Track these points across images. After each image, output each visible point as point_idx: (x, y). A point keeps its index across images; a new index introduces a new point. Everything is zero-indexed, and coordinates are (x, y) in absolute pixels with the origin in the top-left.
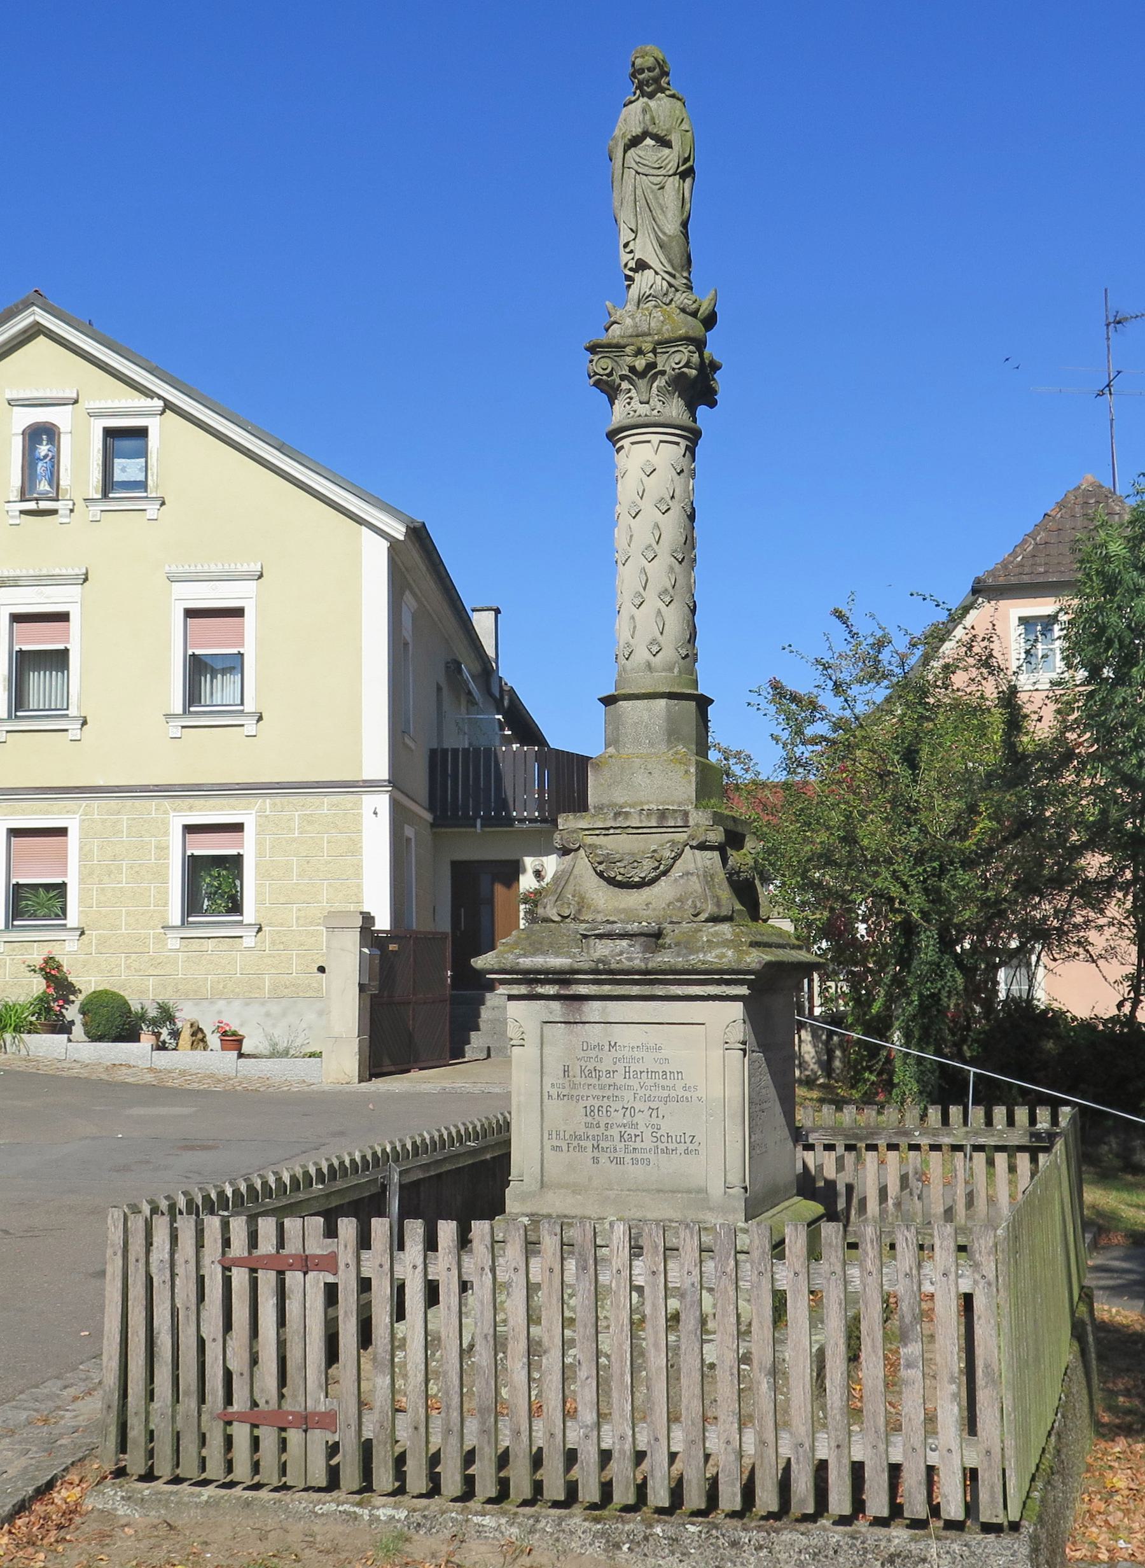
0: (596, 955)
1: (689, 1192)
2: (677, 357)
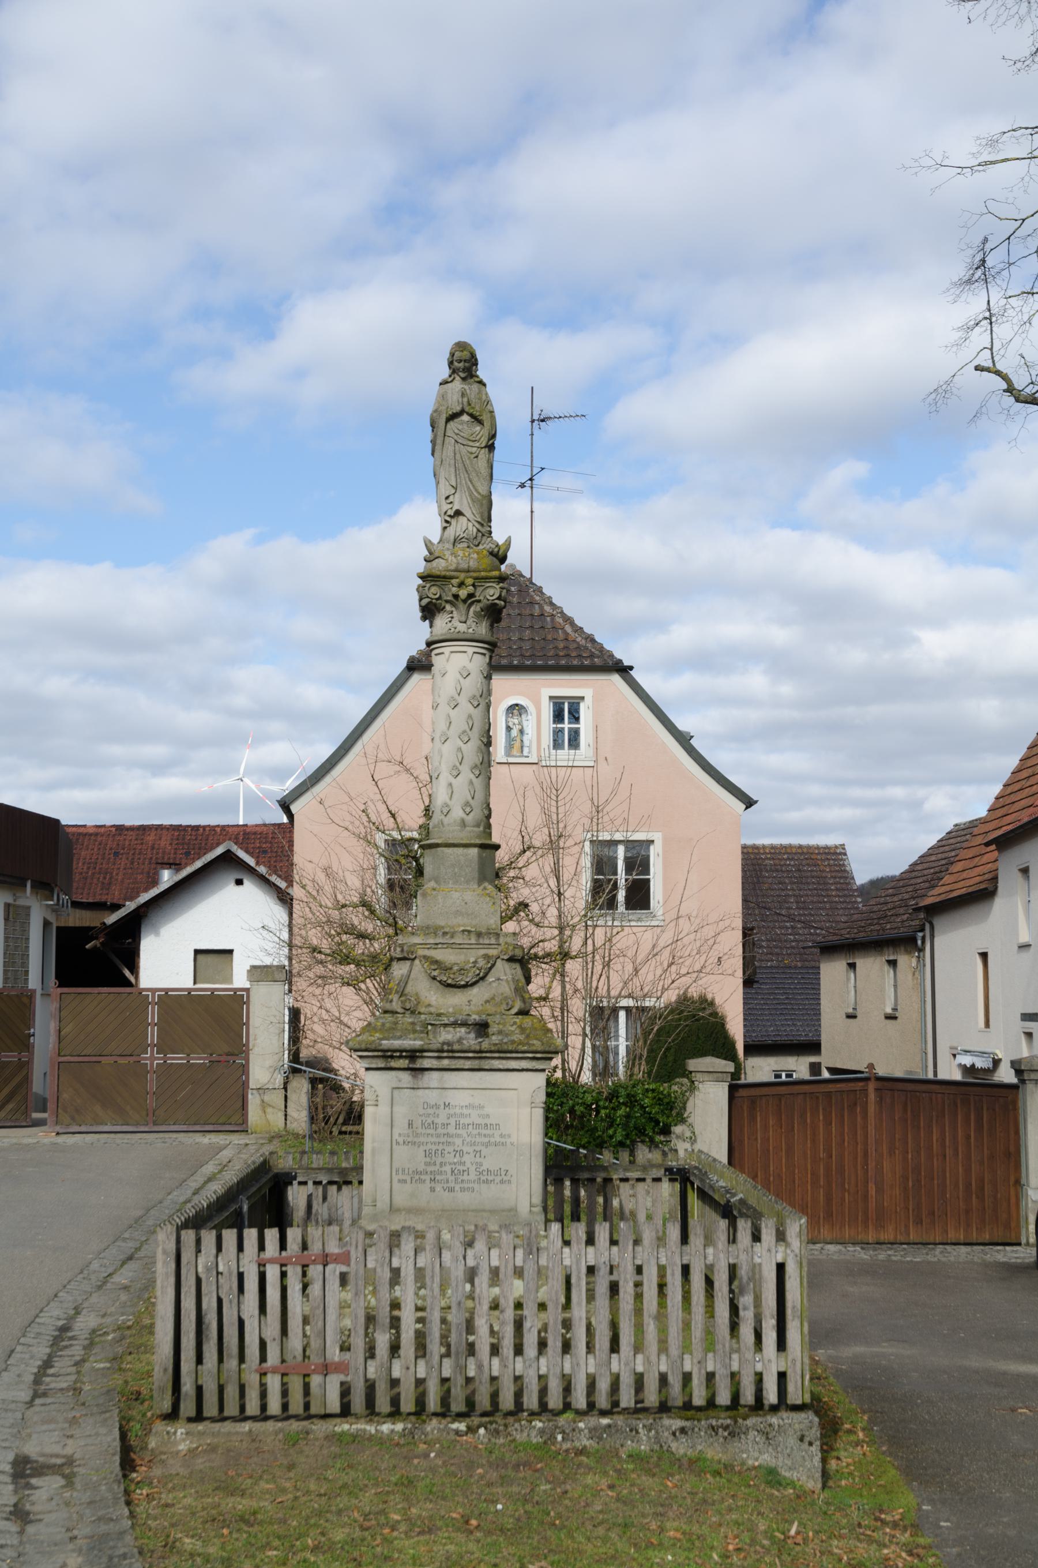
0: (441, 1039)
1: (503, 1211)
2: (491, 591)
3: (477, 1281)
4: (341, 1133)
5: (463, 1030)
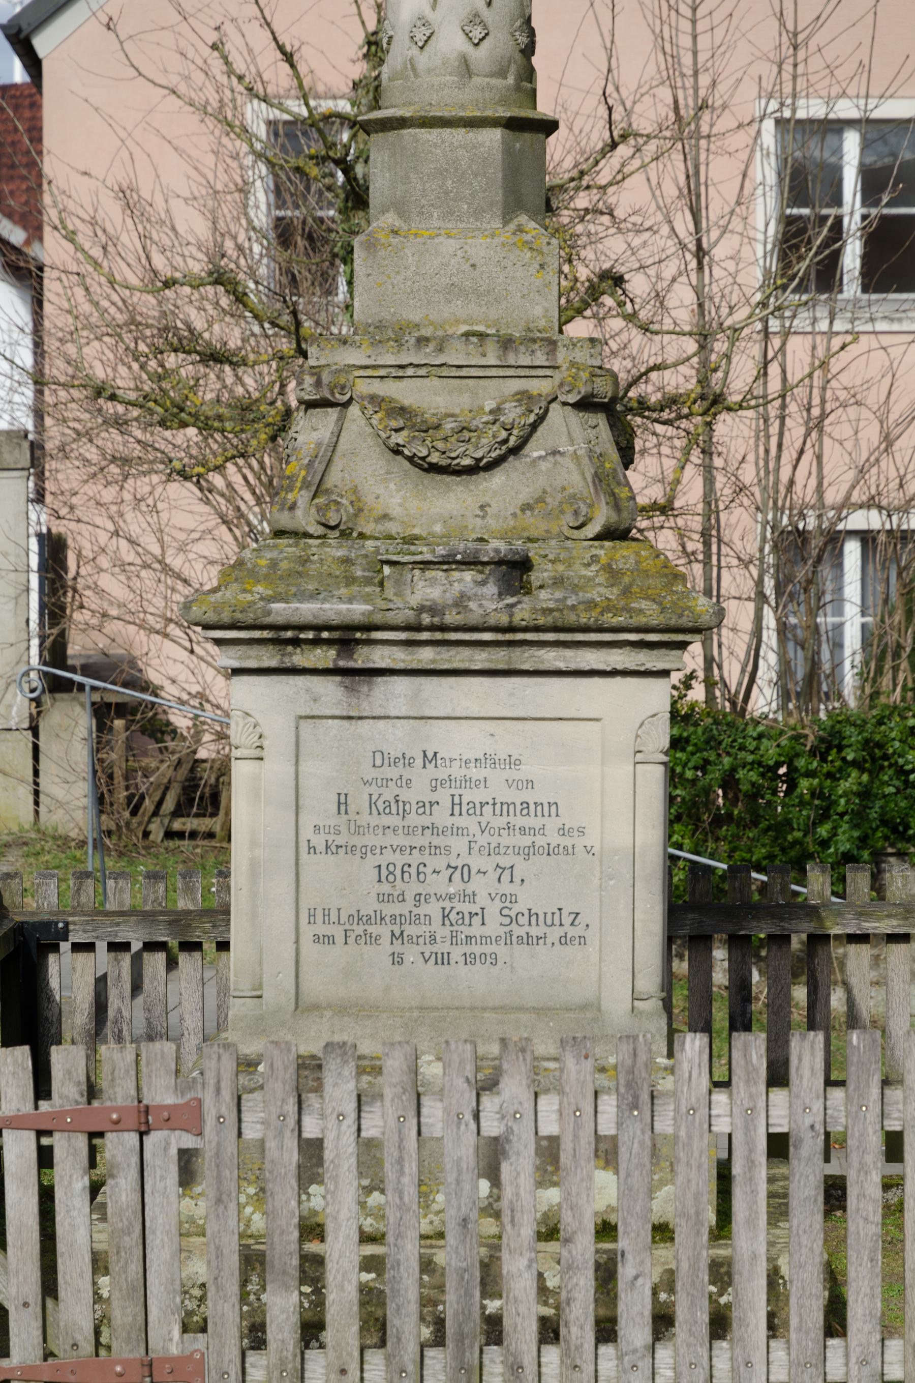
0: (415, 600)
1: (568, 1010)
3: (506, 1170)
4: (170, 835)
5: (468, 576)
